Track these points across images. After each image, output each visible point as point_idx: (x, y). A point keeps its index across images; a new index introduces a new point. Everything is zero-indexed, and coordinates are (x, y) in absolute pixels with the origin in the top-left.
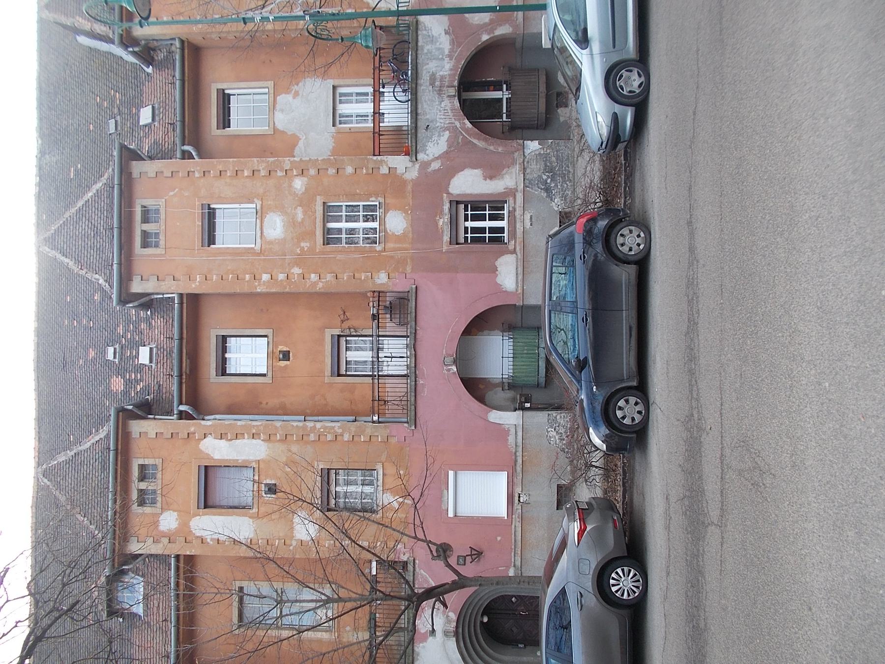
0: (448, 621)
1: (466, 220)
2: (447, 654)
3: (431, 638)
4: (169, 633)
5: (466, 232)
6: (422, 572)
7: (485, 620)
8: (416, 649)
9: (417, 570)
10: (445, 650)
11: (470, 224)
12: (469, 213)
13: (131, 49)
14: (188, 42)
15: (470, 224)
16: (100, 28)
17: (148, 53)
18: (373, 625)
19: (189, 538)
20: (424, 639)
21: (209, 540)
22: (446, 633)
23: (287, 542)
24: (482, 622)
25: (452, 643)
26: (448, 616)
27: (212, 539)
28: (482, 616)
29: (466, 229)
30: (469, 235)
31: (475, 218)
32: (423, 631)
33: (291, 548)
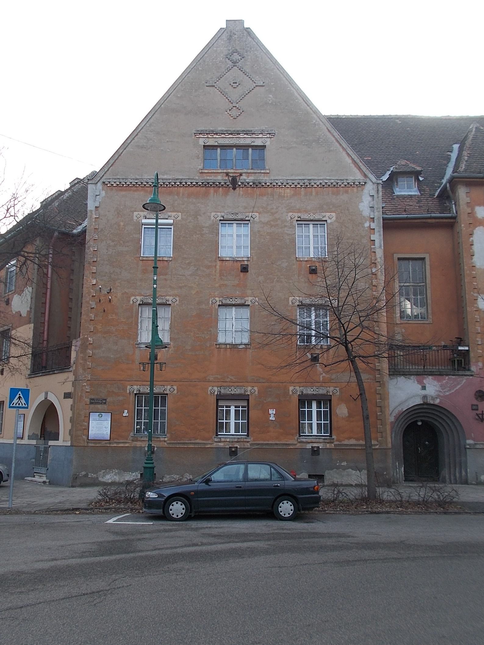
0: (433, 398)
1: (236, 407)
2: (411, 398)
3: (420, 387)
4: (397, 213)
5: (227, 407)
6: (464, 381)
7: (420, 423)
8: (412, 377)
9: (465, 377)
10: (414, 396)
11: (233, 409)
12: (241, 409)
13: (448, 185)
14: (455, 222)
15: (233, 409)
16: (463, 167)
17: (446, 197)
18: (425, 348)
19: (472, 225)
20: (420, 382)
21: (471, 239)
22: (425, 397)
23: (476, 290)
24: (417, 421)
25: (419, 401)
26: (437, 398)
27: (473, 241)
28: (422, 421)
29: (230, 407)
30: (225, 409)
31: (237, 412)
32: (425, 381)
33: (472, 293)
